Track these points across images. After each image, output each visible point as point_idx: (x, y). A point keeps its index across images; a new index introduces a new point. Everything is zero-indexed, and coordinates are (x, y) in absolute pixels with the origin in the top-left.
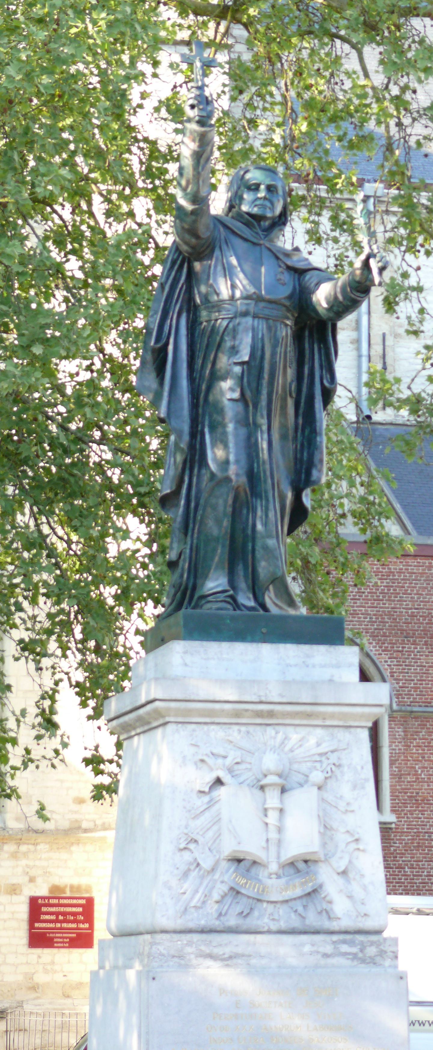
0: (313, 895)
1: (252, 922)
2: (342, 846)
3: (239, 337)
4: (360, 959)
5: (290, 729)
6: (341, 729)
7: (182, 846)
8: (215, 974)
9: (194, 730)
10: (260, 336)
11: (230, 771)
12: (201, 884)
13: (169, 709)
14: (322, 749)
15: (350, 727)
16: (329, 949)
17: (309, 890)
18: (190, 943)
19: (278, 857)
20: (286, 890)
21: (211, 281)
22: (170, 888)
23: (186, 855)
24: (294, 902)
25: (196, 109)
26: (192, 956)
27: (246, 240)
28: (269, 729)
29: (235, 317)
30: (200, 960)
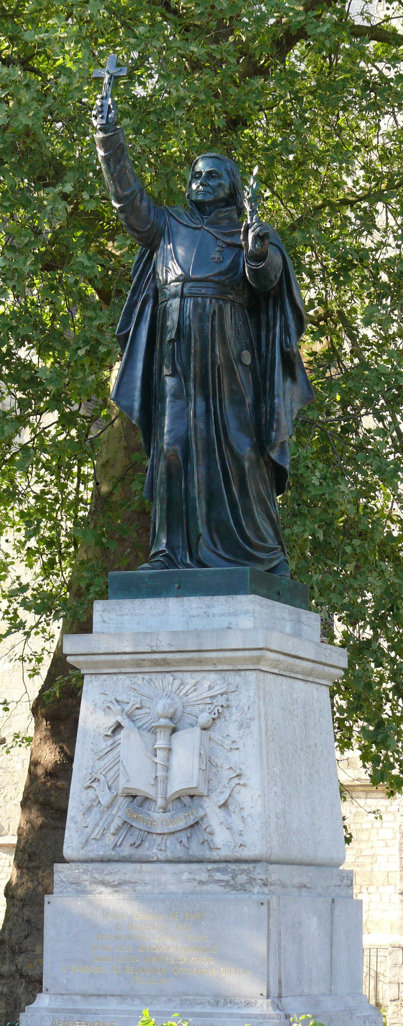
0: (196, 826)
1: (142, 852)
4: (232, 886)
5: (187, 675)
6: (232, 673)
8: (108, 899)
11: (130, 716)
12: (101, 819)
14: (211, 693)
16: (204, 877)
17: (192, 823)
18: (85, 872)
23: (91, 791)
24: (179, 834)
26: (87, 883)
27: (187, 226)
28: (168, 675)
30: (94, 886)
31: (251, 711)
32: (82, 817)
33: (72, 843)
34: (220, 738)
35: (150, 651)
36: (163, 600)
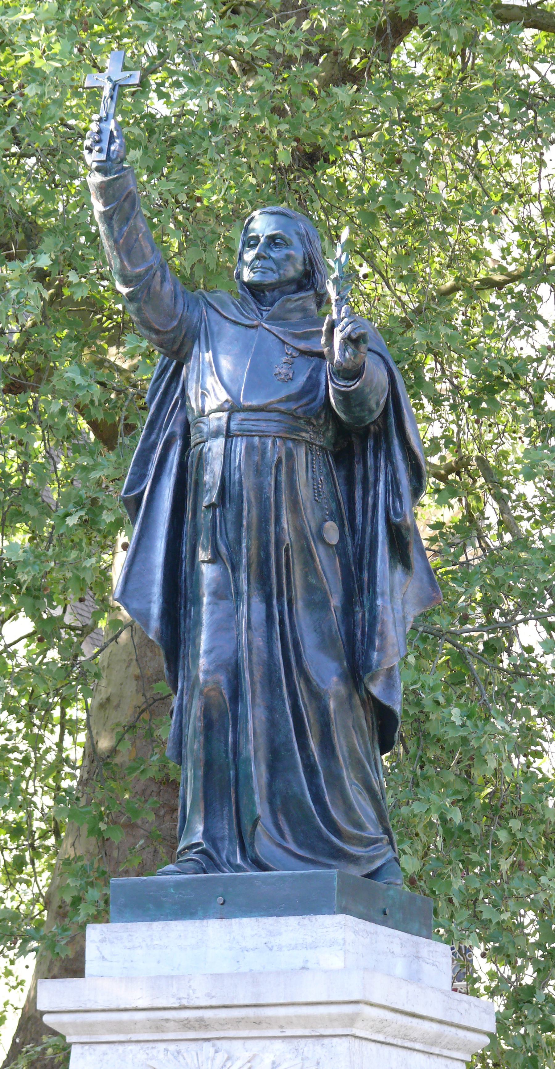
5: (238, 1044)
6: (310, 1041)
15: (441, 1022)
27: (235, 323)
35: (177, 1005)
36: (197, 923)
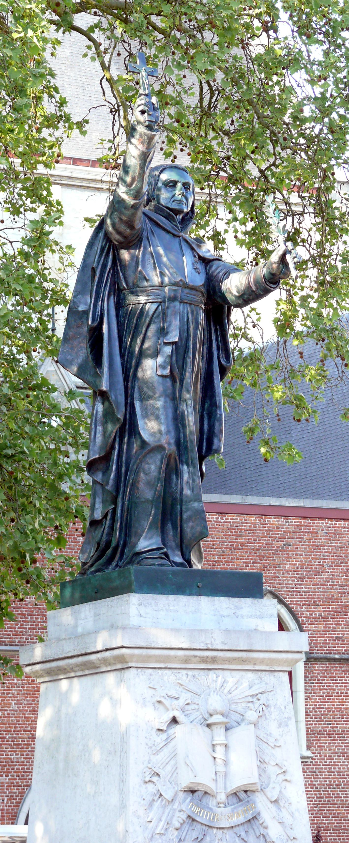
2: (273, 777)
3: (168, 319)
5: (227, 673)
6: (267, 673)
7: (147, 779)
9: (151, 675)
10: (186, 320)
12: (163, 813)
13: (132, 656)
15: (275, 671)
19: (225, 788)
20: (232, 817)
21: (140, 268)
22: (139, 817)
23: (150, 786)
24: (237, 828)
25: (146, 115)
27: (168, 232)
28: (211, 673)
29: (164, 301)
31: (287, 710)
32: (145, 811)
33: (137, 838)
34: (265, 736)
35: (205, 648)
36: (195, 598)
